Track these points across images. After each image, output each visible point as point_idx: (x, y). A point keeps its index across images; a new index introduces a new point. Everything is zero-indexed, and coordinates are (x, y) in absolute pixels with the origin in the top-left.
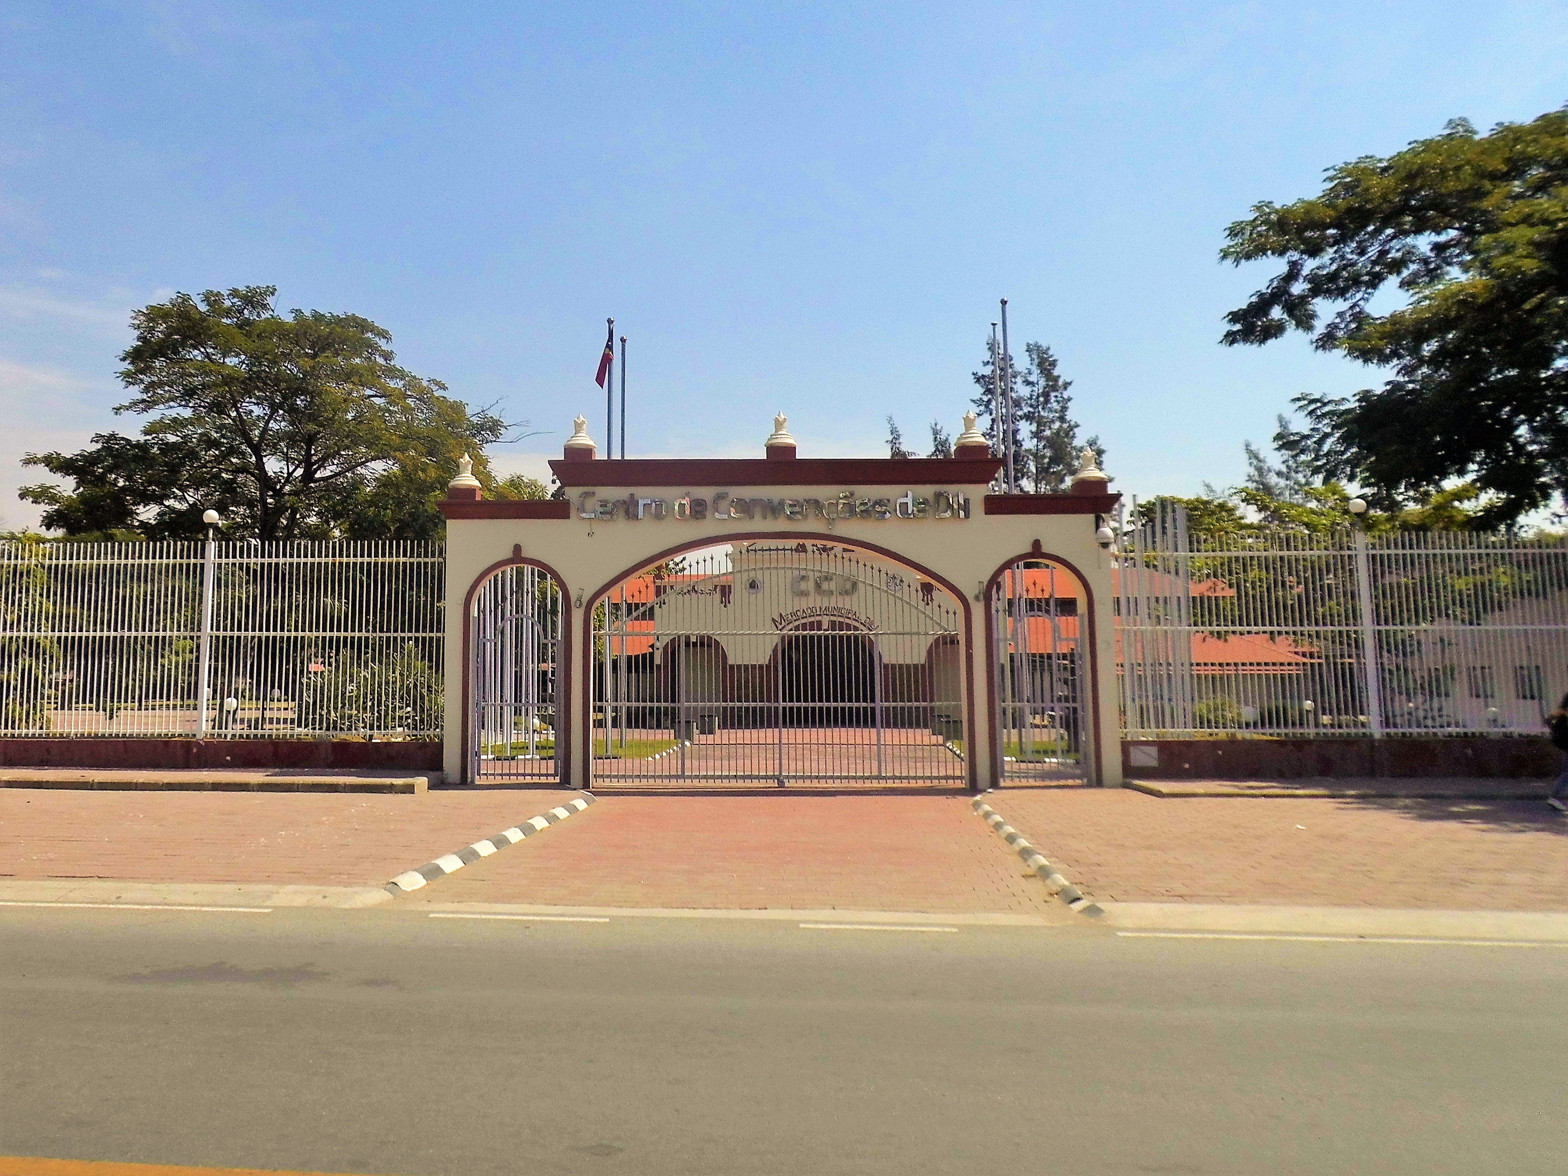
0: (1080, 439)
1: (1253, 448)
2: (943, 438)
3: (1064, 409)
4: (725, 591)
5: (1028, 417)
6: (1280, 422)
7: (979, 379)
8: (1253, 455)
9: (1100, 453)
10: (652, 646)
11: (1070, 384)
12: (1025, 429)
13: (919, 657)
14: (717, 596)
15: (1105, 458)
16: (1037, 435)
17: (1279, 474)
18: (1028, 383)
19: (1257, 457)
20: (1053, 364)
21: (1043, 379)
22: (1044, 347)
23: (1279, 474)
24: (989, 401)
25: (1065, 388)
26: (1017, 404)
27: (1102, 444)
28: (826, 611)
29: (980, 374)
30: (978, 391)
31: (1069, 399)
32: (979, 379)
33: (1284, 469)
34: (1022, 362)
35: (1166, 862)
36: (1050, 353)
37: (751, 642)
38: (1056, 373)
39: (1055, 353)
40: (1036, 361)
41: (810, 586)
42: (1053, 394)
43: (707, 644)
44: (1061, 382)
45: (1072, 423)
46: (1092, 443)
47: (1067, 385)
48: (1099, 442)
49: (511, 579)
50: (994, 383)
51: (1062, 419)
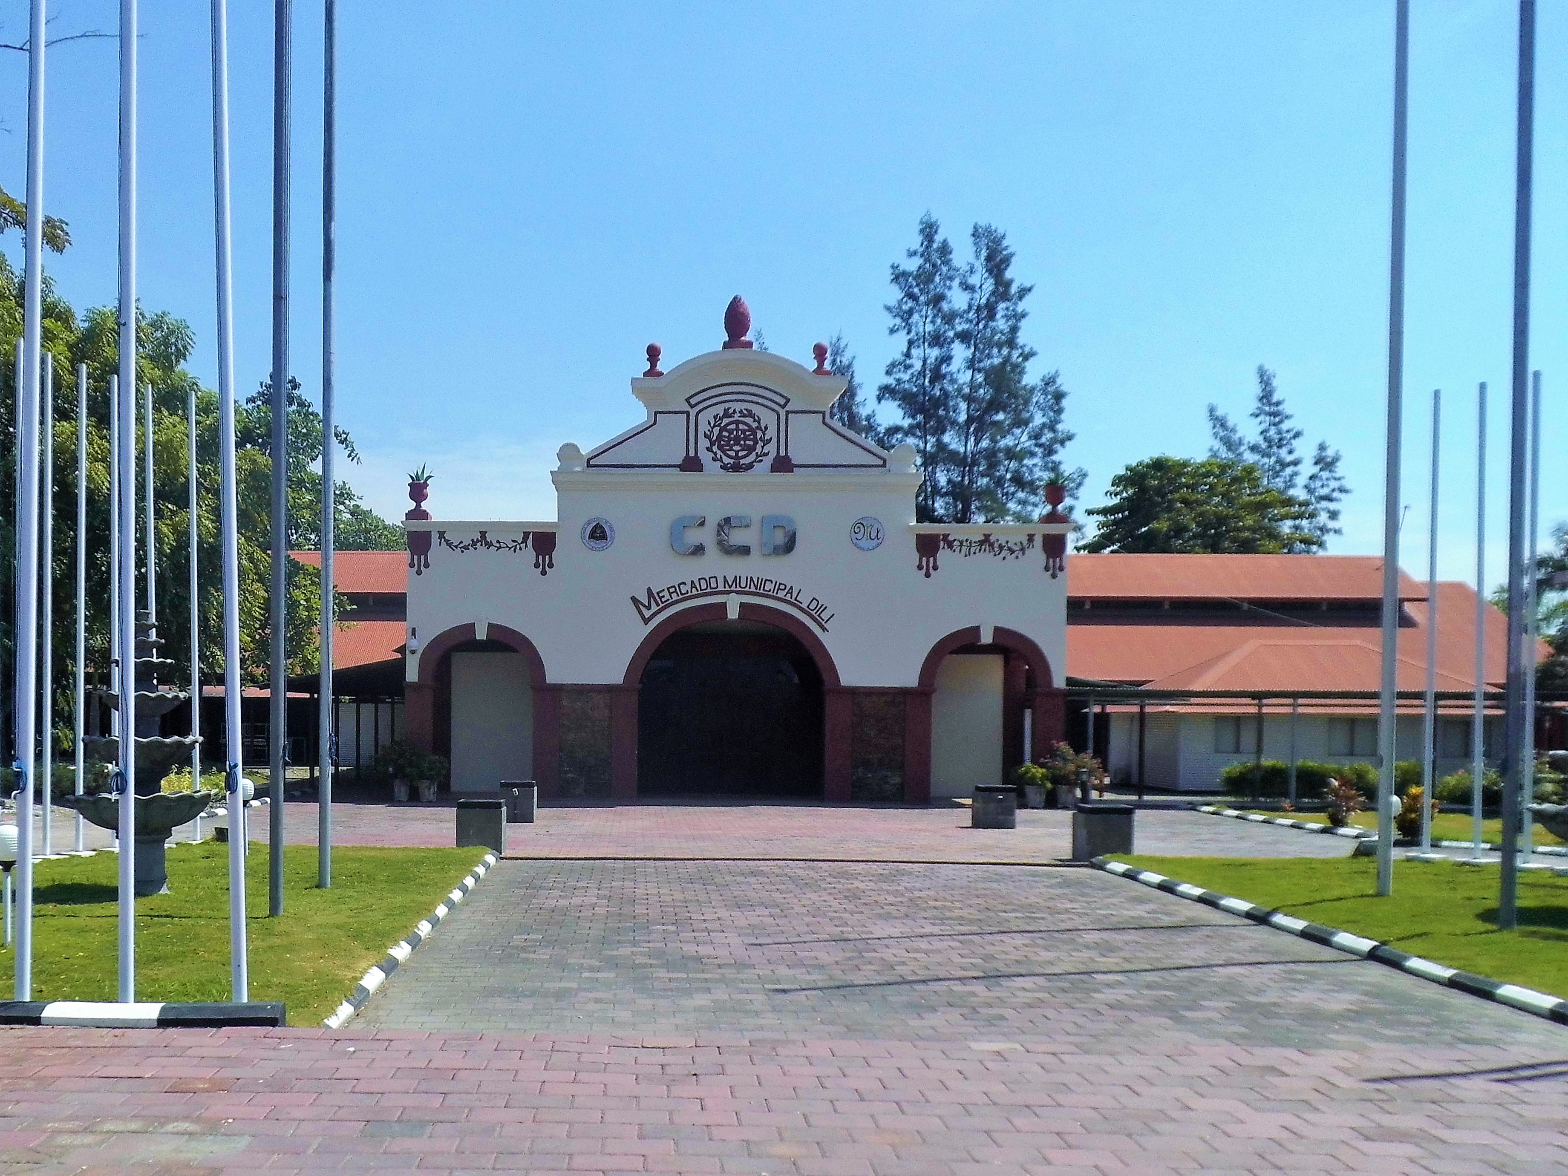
0: (1032, 375)
1: (1219, 413)
2: (845, 361)
3: (1014, 330)
4: (543, 542)
5: (964, 337)
6: (1261, 376)
7: (899, 276)
8: (1219, 422)
9: (1059, 396)
10: (402, 650)
11: (1030, 290)
12: (960, 353)
13: (906, 675)
14: (529, 554)
15: (1065, 403)
16: (971, 364)
17: (1254, 448)
18: (967, 287)
19: (1223, 425)
20: (1006, 261)
21: (991, 281)
22: (1001, 231)
23: (1254, 448)
24: (910, 312)
25: (1020, 298)
26: (950, 318)
27: (1064, 383)
28: (734, 586)
29: (901, 268)
30: (894, 294)
31: (1023, 315)
32: (899, 276)
33: (1260, 440)
34: (964, 254)
35: (945, 898)
36: (1005, 243)
37: (592, 644)
38: (1008, 274)
39: (1010, 243)
40: (984, 253)
41: (706, 536)
42: (1002, 305)
43: (506, 644)
44: (1014, 289)
45: (1027, 350)
46: (1049, 381)
47: (1024, 292)
48: (1059, 381)
49: (42, 462)
50: (922, 282)
51: (1011, 343)
